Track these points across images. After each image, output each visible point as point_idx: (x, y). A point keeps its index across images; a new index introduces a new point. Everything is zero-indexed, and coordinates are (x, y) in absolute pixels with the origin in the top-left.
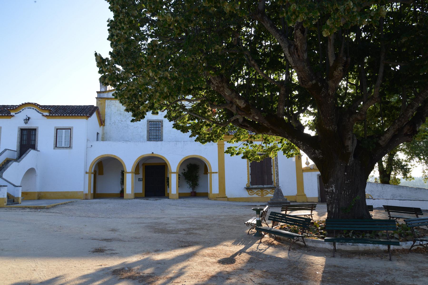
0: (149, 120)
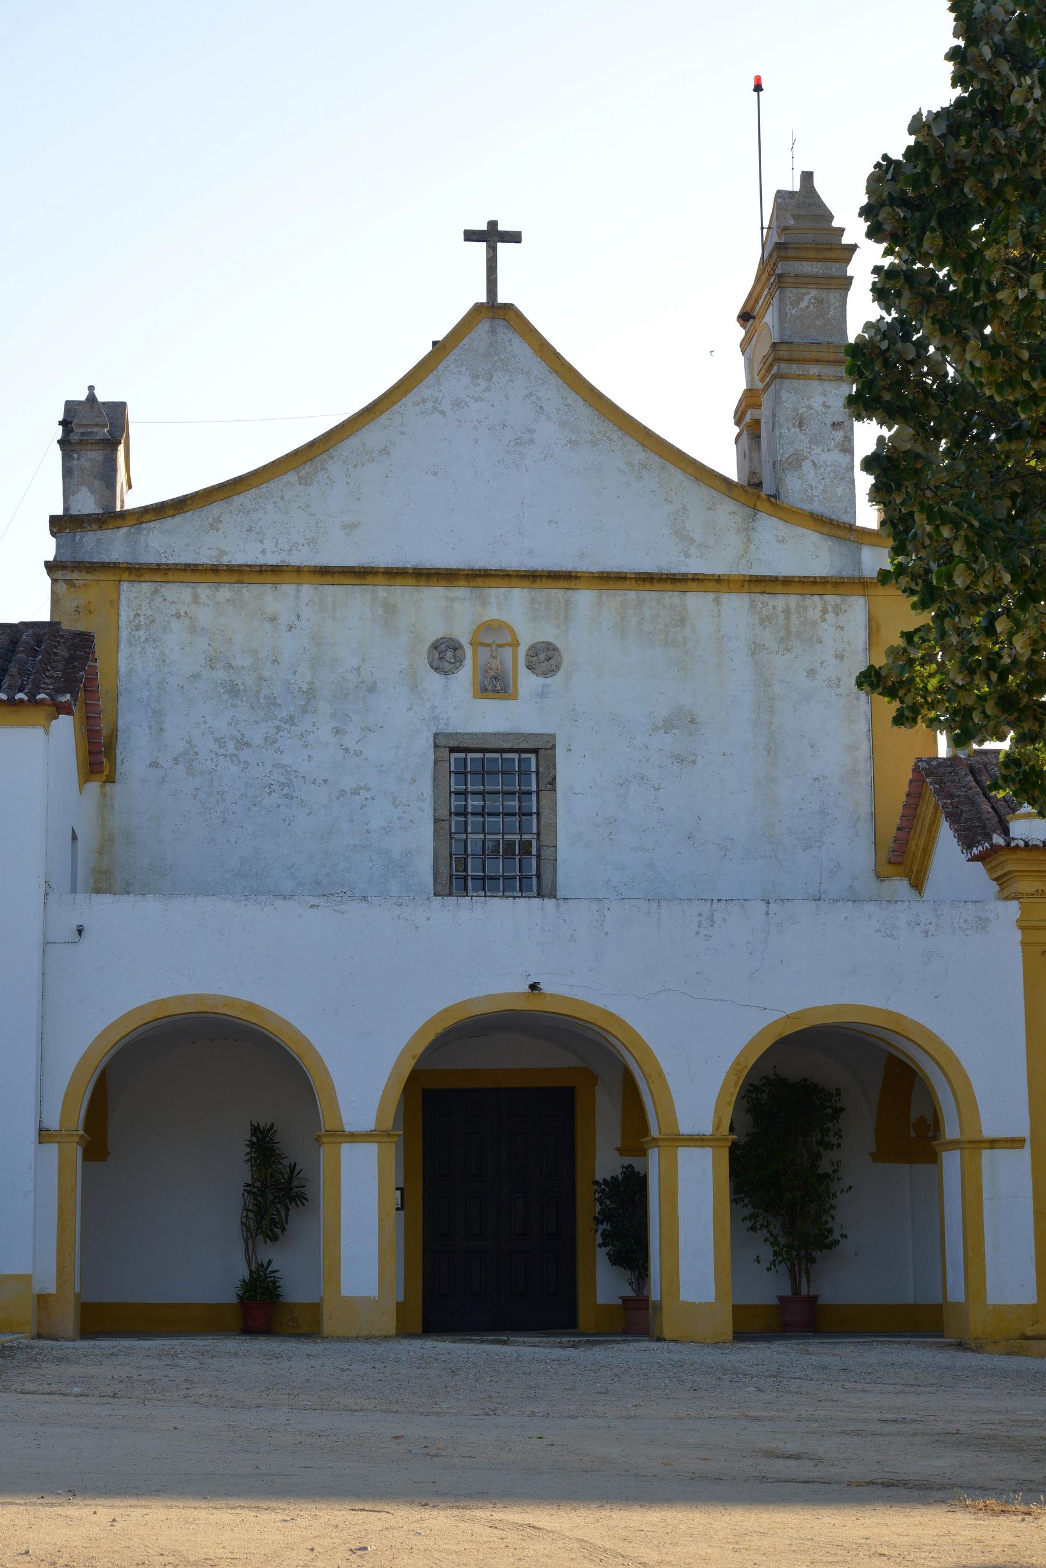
0: (449, 735)
